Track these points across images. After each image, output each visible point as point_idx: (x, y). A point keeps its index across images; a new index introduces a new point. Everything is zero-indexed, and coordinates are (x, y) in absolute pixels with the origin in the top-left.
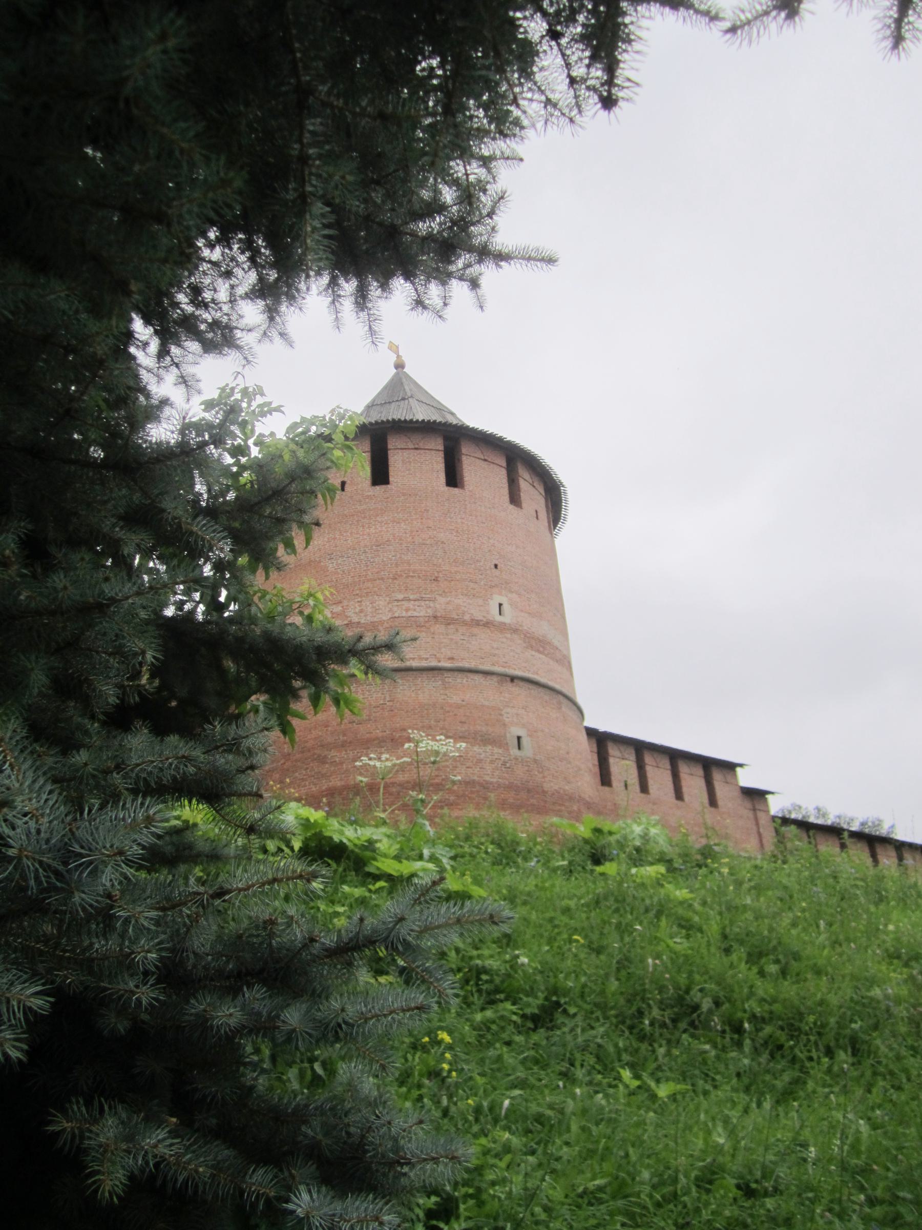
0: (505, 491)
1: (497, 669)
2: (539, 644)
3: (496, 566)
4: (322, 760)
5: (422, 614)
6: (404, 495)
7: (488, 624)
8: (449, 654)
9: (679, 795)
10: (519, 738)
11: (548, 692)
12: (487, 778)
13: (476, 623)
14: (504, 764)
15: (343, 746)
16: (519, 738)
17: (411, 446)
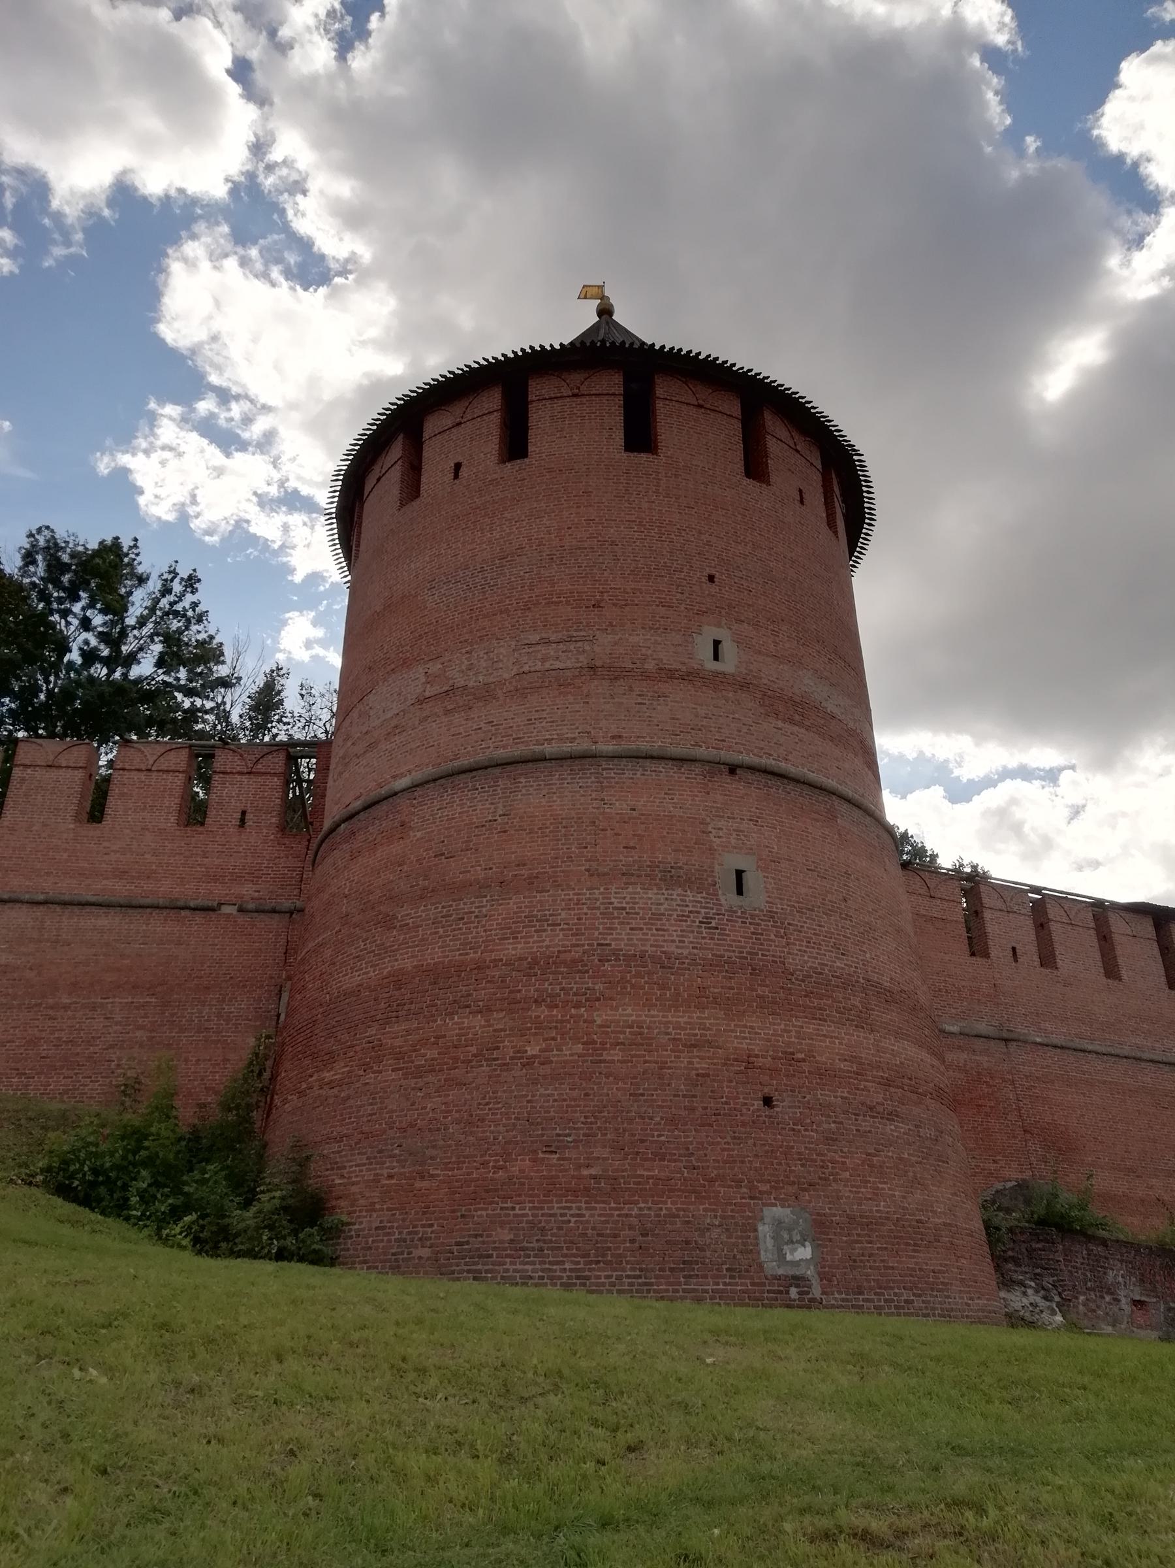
0: (738, 456)
1: (702, 752)
2: (797, 710)
3: (711, 578)
4: (388, 922)
5: (569, 664)
6: (550, 471)
7: (691, 676)
8: (614, 730)
9: (1111, 970)
10: (739, 874)
11: (807, 791)
12: (671, 948)
13: (669, 675)
14: (706, 921)
15: (422, 898)
16: (739, 874)
17: (566, 391)
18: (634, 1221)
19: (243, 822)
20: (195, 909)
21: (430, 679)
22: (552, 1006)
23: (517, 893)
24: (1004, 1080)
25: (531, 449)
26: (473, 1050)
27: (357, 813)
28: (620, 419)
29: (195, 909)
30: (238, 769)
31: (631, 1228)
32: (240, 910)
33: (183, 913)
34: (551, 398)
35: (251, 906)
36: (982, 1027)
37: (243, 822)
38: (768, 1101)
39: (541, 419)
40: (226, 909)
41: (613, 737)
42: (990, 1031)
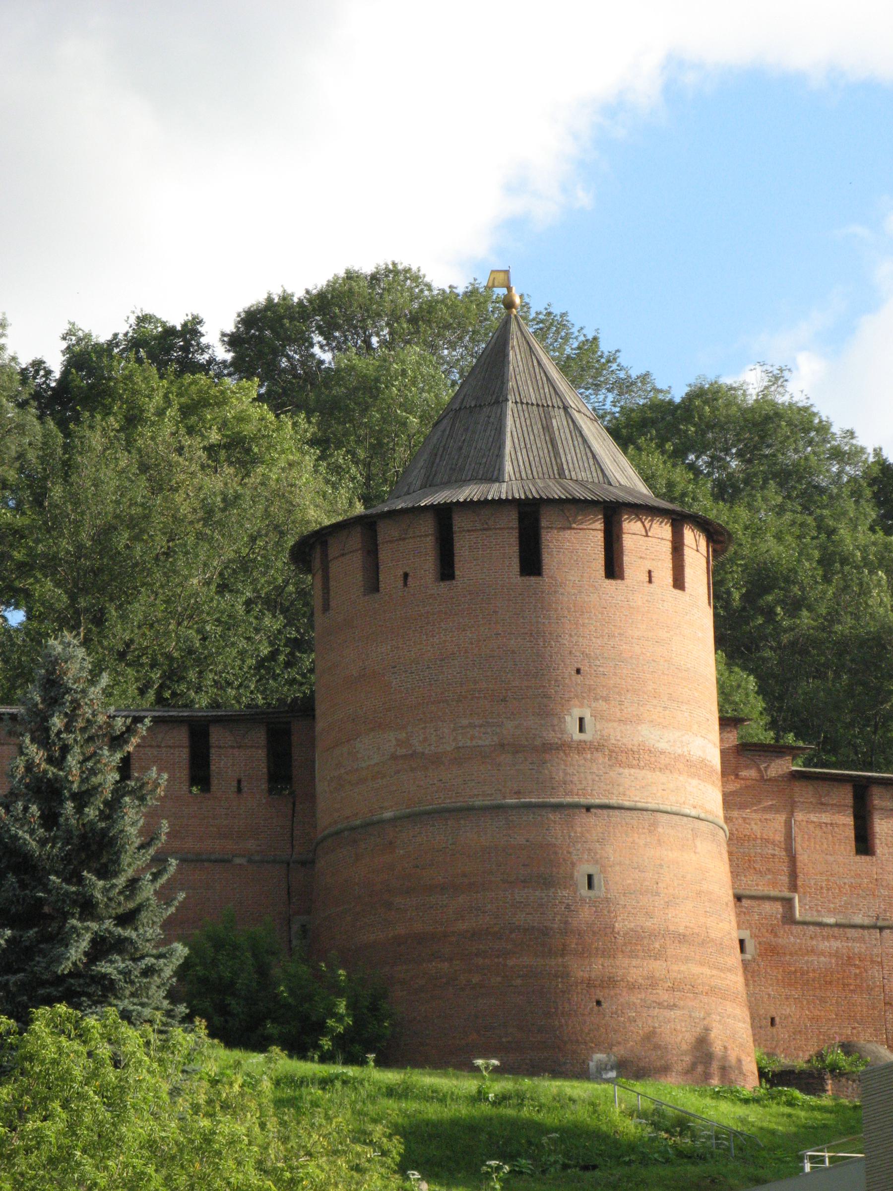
5: (487, 743)
18: (528, 1061)
19: (239, 790)
20: (216, 861)
21: (400, 743)
24: (872, 962)
25: (457, 573)
26: (444, 980)
28: (516, 549)
29: (216, 861)
31: (527, 1064)
32: (250, 861)
34: (468, 531)
35: (257, 858)
36: (858, 919)
37: (239, 790)
38: (599, 1003)
39: (462, 546)
40: (237, 861)
41: (516, 793)
42: (867, 921)
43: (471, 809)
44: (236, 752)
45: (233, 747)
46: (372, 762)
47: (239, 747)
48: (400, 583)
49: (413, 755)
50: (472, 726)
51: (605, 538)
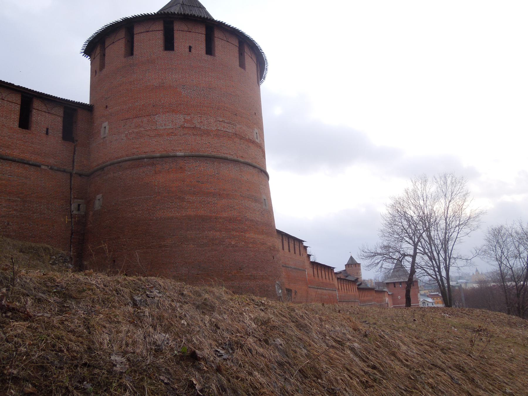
5: (230, 131)
19: (47, 133)
21: (186, 121)
22: (236, 232)
23: (224, 198)
27: (156, 158)
30: (44, 110)
33: (26, 166)
35: (55, 168)
37: (47, 133)
40: (43, 167)
43: (226, 159)
44: (47, 115)
45: (45, 112)
46: (168, 127)
47: (49, 113)
48: (188, 50)
49: (194, 128)
50: (223, 121)
51: (21, 109)
